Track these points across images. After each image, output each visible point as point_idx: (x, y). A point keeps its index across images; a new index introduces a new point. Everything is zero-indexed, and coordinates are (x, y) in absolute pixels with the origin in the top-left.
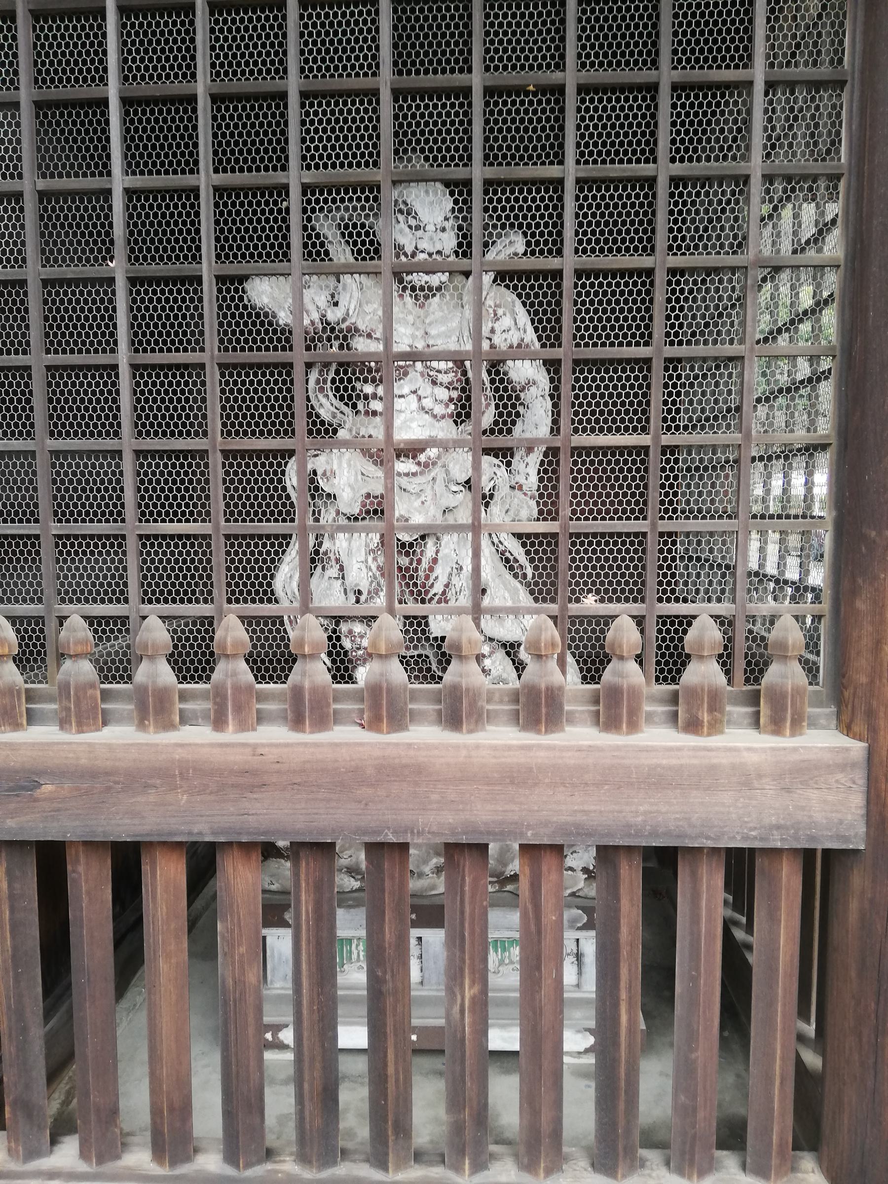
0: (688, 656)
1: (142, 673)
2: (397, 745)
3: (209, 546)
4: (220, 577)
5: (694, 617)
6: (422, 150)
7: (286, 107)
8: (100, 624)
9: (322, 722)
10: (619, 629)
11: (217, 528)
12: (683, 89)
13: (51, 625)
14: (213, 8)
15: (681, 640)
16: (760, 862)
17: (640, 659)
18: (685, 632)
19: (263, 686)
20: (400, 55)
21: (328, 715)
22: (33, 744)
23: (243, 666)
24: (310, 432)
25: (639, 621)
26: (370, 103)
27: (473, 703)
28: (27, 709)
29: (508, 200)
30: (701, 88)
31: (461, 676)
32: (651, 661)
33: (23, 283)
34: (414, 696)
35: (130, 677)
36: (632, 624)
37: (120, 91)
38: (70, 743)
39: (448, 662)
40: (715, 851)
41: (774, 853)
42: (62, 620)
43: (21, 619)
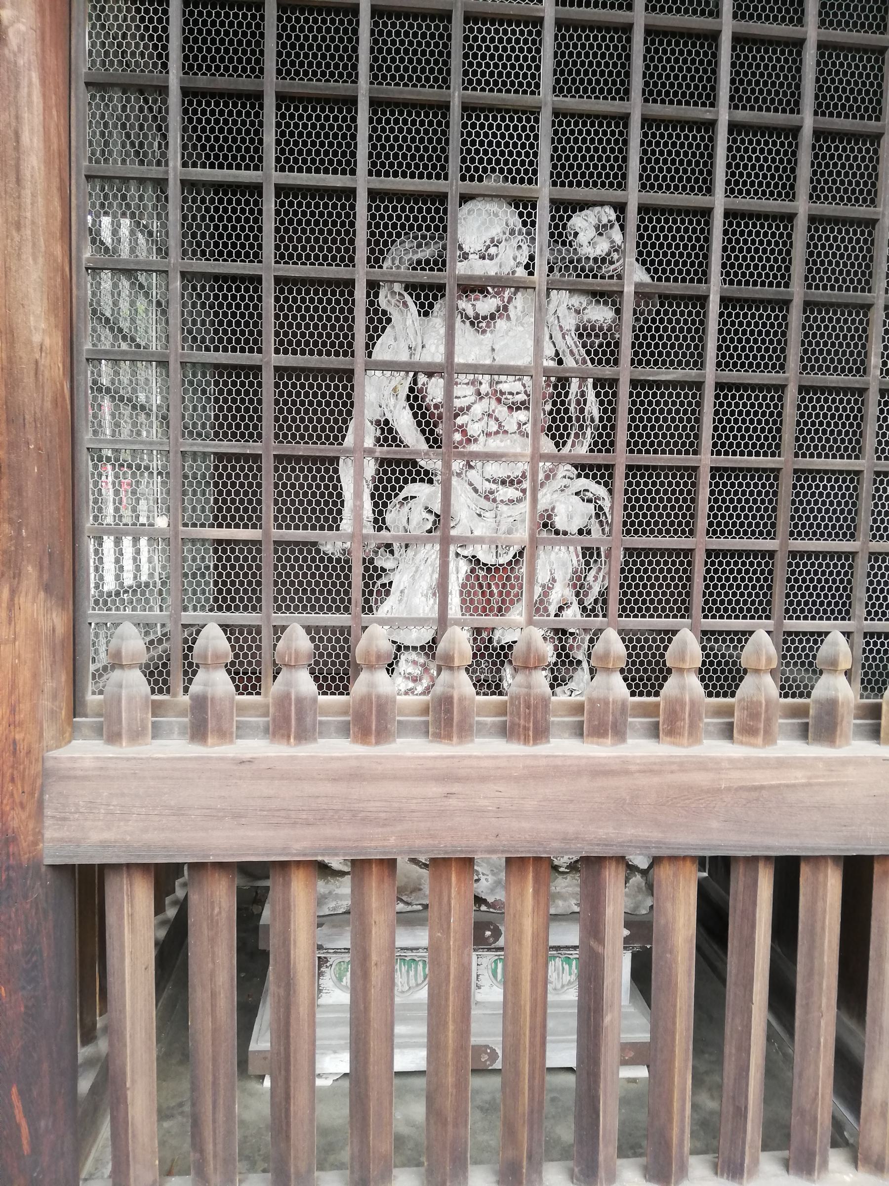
0: (669, 671)
1: (671, 686)
2: (222, 759)
3: (259, 551)
4: (860, 595)
5: (827, 634)
6: (501, 171)
7: (261, 107)
8: (317, 633)
9: (304, 735)
10: (607, 642)
11: (267, 534)
12: (195, 94)
13: (266, 635)
14: (186, 1)
15: (662, 656)
16: (805, 871)
17: (848, 673)
18: (666, 648)
19: (245, 698)
20: (284, 63)
21: (471, 726)
22: (509, 757)
23: (768, 680)
24: (277, 436)
25: (848, 635)
26: (253, 106)
27: (219, 717)
28: (153, 723)
29: (766, 234)
30: (213, 96)
31: (121, 686)
32: (859, 674)
33: (258, 279)
34: (242, 709)
35: (346, 688)
36: (842, 639)
37: (182, 80)
38: (453, 757)
39: (195, 673)
40: (767, 858)
41: (817, 860)
42: (279, 630)
43: (317, 629)
